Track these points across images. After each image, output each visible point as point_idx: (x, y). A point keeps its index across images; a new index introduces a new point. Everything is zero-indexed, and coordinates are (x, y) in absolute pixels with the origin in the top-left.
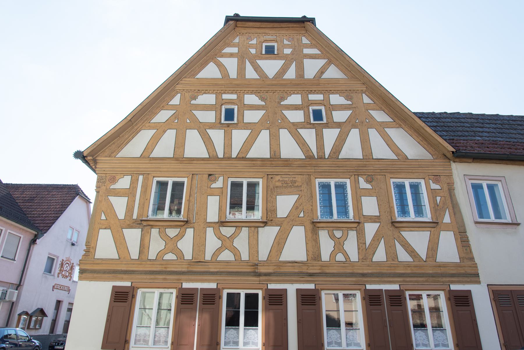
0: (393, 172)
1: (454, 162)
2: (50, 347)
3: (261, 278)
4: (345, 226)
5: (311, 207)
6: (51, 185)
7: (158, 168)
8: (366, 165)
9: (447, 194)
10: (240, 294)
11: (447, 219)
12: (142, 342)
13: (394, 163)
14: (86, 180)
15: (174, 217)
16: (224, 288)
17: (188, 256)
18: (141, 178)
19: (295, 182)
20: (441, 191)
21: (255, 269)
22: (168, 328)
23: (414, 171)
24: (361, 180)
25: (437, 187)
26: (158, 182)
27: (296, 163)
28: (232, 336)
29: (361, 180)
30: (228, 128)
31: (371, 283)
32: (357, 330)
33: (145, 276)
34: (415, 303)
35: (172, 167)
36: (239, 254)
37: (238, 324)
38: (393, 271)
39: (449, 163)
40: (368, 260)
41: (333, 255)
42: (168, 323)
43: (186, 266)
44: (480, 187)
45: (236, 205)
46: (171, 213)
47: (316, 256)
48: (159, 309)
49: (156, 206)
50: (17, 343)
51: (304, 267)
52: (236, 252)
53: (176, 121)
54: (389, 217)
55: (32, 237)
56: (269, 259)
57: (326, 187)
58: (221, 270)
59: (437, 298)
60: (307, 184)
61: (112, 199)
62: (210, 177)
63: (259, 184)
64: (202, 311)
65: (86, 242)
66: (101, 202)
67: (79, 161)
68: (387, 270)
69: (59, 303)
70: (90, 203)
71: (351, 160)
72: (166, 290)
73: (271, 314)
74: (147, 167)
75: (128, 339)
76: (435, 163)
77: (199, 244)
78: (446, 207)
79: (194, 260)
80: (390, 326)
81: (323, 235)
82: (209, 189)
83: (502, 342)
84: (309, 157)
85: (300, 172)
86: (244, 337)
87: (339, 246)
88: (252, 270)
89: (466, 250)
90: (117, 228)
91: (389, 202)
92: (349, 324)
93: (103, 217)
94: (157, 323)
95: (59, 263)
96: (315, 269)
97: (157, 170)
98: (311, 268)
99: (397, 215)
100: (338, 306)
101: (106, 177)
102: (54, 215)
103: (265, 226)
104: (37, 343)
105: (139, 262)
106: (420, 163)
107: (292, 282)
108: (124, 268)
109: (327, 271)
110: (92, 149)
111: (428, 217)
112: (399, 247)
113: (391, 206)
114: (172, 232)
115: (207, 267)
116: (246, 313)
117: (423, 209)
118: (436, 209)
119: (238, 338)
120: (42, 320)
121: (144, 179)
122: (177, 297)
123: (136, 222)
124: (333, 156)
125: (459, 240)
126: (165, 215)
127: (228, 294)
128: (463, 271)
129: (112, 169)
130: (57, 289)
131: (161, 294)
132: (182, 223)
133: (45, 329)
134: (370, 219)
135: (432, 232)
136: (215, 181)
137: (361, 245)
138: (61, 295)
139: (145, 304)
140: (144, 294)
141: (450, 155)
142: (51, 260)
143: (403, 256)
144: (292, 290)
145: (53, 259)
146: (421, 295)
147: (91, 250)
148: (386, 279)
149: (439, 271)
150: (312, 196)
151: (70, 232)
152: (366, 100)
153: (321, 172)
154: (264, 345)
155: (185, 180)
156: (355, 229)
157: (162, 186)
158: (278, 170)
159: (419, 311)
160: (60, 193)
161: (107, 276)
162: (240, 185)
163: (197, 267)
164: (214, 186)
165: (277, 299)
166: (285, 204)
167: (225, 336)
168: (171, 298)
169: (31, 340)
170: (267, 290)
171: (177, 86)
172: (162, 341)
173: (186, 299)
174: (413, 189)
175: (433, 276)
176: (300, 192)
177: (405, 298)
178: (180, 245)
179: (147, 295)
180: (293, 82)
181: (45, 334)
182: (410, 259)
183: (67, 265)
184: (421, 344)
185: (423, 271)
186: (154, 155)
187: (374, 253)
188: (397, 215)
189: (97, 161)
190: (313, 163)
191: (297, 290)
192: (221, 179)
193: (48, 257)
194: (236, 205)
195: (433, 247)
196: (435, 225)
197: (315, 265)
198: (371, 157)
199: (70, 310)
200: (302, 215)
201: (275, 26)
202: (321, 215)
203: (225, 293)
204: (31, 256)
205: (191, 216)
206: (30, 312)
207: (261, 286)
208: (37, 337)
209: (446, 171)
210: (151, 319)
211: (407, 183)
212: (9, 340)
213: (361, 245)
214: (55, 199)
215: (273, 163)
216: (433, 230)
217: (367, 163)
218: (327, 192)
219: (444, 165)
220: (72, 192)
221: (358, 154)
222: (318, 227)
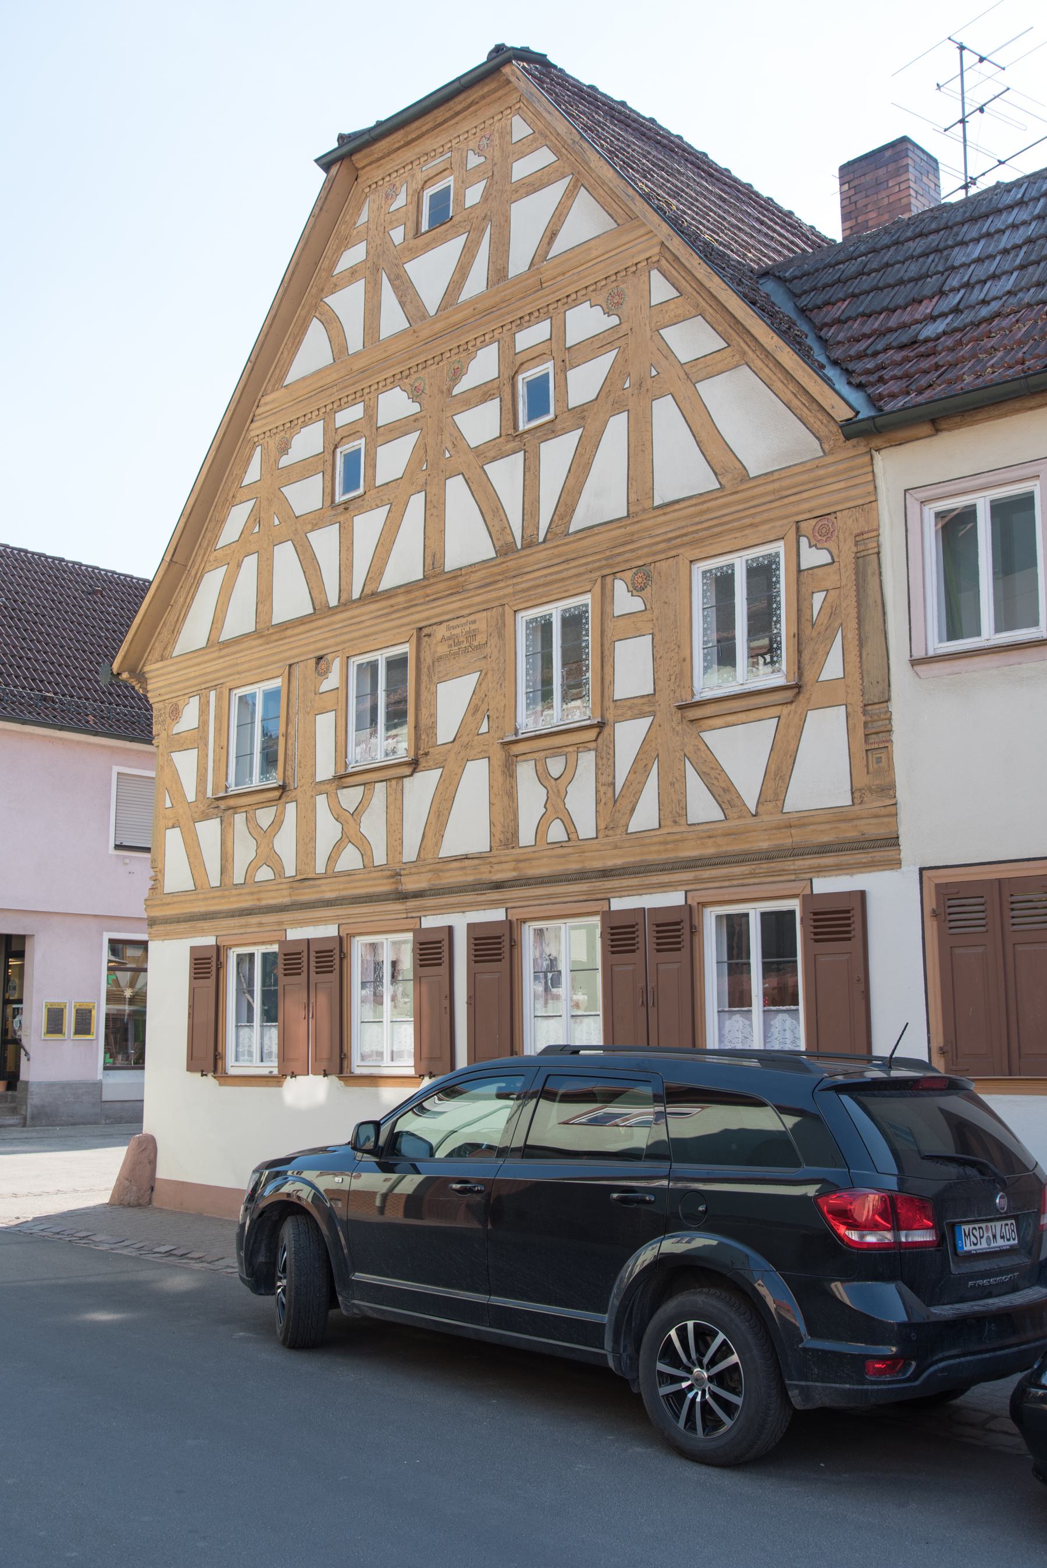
0: (702, 540)
8: (633, 534)
11: (833, 667)
18: (213, 694)
19: (472, 635)
23: (758, 519)
24: (620, 587)
27: (474, 577)
29: (620, 587)
30: (347, 516)
31: (622, 892)
35: (256, 656)
36: (369, 853)
38: (671, 855)
40: (619, 832)
47: (509, 836)
53: (257, 529)
68: (659, 852)
74: (218, 667)
76: (821, 472)
78: (837, 624)
79: (299, 877)
81: (525, 771)
98: (496, 867)
106: (776, 485)
108: (201, 908)
112: (694, 784)
121: (219, 699)
125: (860, 732)
128: (852, 834)
134: (630, 708)
137: (603, 789)
140: (540, 933)
143: (702, 807)
152: (661, 290)
153: (528, 589)
156: (593, 745)
171: (253, 425)
175: (768, 856)
176: (484, 662)
180: (480, 307)
186: (278, 618)
187: (633, 810)
189: (147, 676)
190: (522, 558)
195: (779, 770)
197: (503, 859)
200: (484, 728)
201: (459, 107)
213: (603, 789)
215: (428, 591)
216: (785, 710)
217: (636, 527)
219: (852, 469)
221: (700, 479)
222: (517, 756)
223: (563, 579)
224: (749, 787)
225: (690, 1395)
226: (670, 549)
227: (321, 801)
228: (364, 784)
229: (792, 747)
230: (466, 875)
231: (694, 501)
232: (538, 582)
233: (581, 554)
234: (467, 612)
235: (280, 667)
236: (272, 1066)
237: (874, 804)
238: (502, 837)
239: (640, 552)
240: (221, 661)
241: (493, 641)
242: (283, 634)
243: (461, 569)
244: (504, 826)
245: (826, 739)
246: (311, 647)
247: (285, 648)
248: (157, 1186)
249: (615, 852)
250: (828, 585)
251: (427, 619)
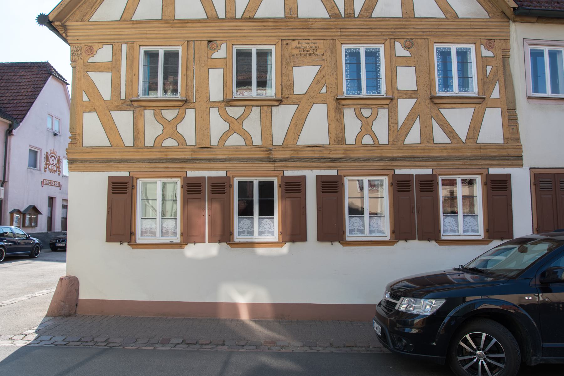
0: (439, 35)
1: (514, 22)
2: (51, 244)
3: (277, 164)
4: (375, 103)
5: (335, 81)
6: (16, 63)
7: (144, 34)
8: (406, 25)
9: (499, 63)
10: (252, 182)
11: (496, 94)
12: (148, 234)
13: (440, 23)
14: (55, 52)
15: (170, 96)
16: (234, 177)
17: (191, 140)
18: (124, 47)
19: (316, 49)
20: (493, 59)
21: (269, 154)
22: (176, 219)
23: (463, 34)
24: (398, 45)
25: (490, 54)
26: (146, 53)
27: (317, 24)
28: (246, 226)
29: (398, 45)
31: (401, 167)
32: (382, 218)
33: (143, 165)
34: (449, 188)
35: (162, 32)
36: (250, 138)
37: (252, 214)
38: (426, 154)
39: (507, 24)
40: (400, 143)
41: (359, 137)
42: (176, 214)
43: (190, 153)
44: (541, 53)
45: (243, 83)
46: (165, 91)
47: (340, 139)
48: (164, 199)
49: (147, 85)
50: (15, 240)
51: (325, 152)
52: (246, 135)
54: (428, 92)
55: (6, 127)
56: (285, 143)
57: (354, 55)
58: (230, 156)
59: (473, 183)
60: (331, 52)
61: (93, 75)
62: (210, 44)
63: (271, 52)
64: (211, 201)
65: (70, 129)
66: (79, 79)
67: (45, 29)
68: (420, 153)
69: (51, 200)
70: (67, 84)
71: (387, 19)
72: (169, 179)
73: (288, 202)
75: (133, 231)
76: (490, 24)
77: (203, 127)
78: (496, 79)
79: (197, 146)
80: (418, 212)
81: (349, 114)
82: (209, 60)
83: (535, 226)
84: (335, 16)
85: (322, 36)
86: (259, 226)
87: (367, 127)
88: (266, 156)
89: (513, 129)
90: (105, 111)
91: (429, 74)
92: (373, 214)
93: (85, 98)
94: (163, 214)
95: (43, 156)
96: (338, 154)
97: (143, 36)
98: (333, 152)
99: (437, 89)
100: (362, 194)
101: (81, 47)
102: (26, 101)
103: (279, 104)
104: (37, 241)
105: (135, 150)
106: (472, 23)
107: (311, 168)
108: (118, 156)
109: (352, 156)
110: (59, 11)
111: (474, 90)
112: (437, 129)
113: (431, 78)
114: (170, 114)
115: (214, 153)
116: (260, 202)
117: (470, 82)
118: (486, 82)
119: (253, 228)
120: (37, 218)
121: (128, 49)
122: (182, 187)
123: (125, 102)
124: (365, 15)
125: (506, 118)
126: (160, 94)
127: (239, 182)
129: (86, 37)
130: (47, 184)
131: (164, 184)
132: (180, 103)
133: (42, 226)
134: (405, 94)
135: (476, 109)
136: (216, 49)
137: (392, 125)
138: (53, 191)
139: (148, 195)
140: (145, 184)
141: (510, 13)
142: (34, 154)
143: (440, 137)
144: (311, 176)
145: (36, 152)
146: (456, 180)
147: (78, 137)
148: (418, 163)
149: (479, 154)
150: (337, 67)
151: (49, 120)
153: (348, 36)
154: (281, 233)
155: (179, 49)
156: (387, 106)
157: (152, 56)
158: (295, 34)
159: (452, 198)
160: (29, 73)
161: (100, 165)
162: (248, 54)
163: (202, 153)
164: (215, 55)
165: (294, 187)
166: (304, 77)
167: (239, 226)
168: (175, 188)
169: (29, 237)
170: (283, 177)
172: (170, 232)
173: (192, 189)
174: (460, 57)
175: (470, 158)
176: (322, 62)
177: (438, 183)
178: (180, 128)
179: (149, 186)
181: (43, 232)
182: (448, 141)
183: (53, 158)
184: (449, 229)
185: (461, 154)
186: (137, 16)
187: (407, 135)
188: (437, 89)
189: (68, 27)
191: (317, 177)
192: (224, 46)
193: (30, 150)
194: (243, 83)
195: (475, 127)
196: (481, 100)
197: (338, 149)
198: (412, 15)
199: (65, 207)
200: (324, 90)
202: (347, 90)
203: (236, 181)
204: (10, 149)
205: (190, 94)
206: (22, 210)
207: (276, 173)
208: (35, 235)
209: (502, 34)
210: (156, 211)
211: (454, 48)
212: (7, 238)
213: (392, 125)
214: (24, 80)
215: (289, 24)
216: (477, 106)
217: (407, 23)
218: (355, 62)
219: (502, 26)
220: (42, 72)
222: (343, 105)
223: (368, 36)
224: (462, 133)
225: (480, 363)
226: (423, 35)
228: (245, 106)
229: (480, 120)
230: (315, 154)
231: (435, 20)
232: (354, 33)
233: (379, 27)
234: (312, 38)
235: (181, 41)
236: (178, 239)
237: (512, 144)
238: (335, 139)
239: (409, 33)
240: (133, 30)
241: (328, 54)
242: (185, 25)
243: (310, 18)
244: (336, 135)
245: (493, 120)
246: (206, 35)
247: (185, 32)
248: (79, 303)
249: (399, 151)
250: (493, 64)
251: (287, 36)
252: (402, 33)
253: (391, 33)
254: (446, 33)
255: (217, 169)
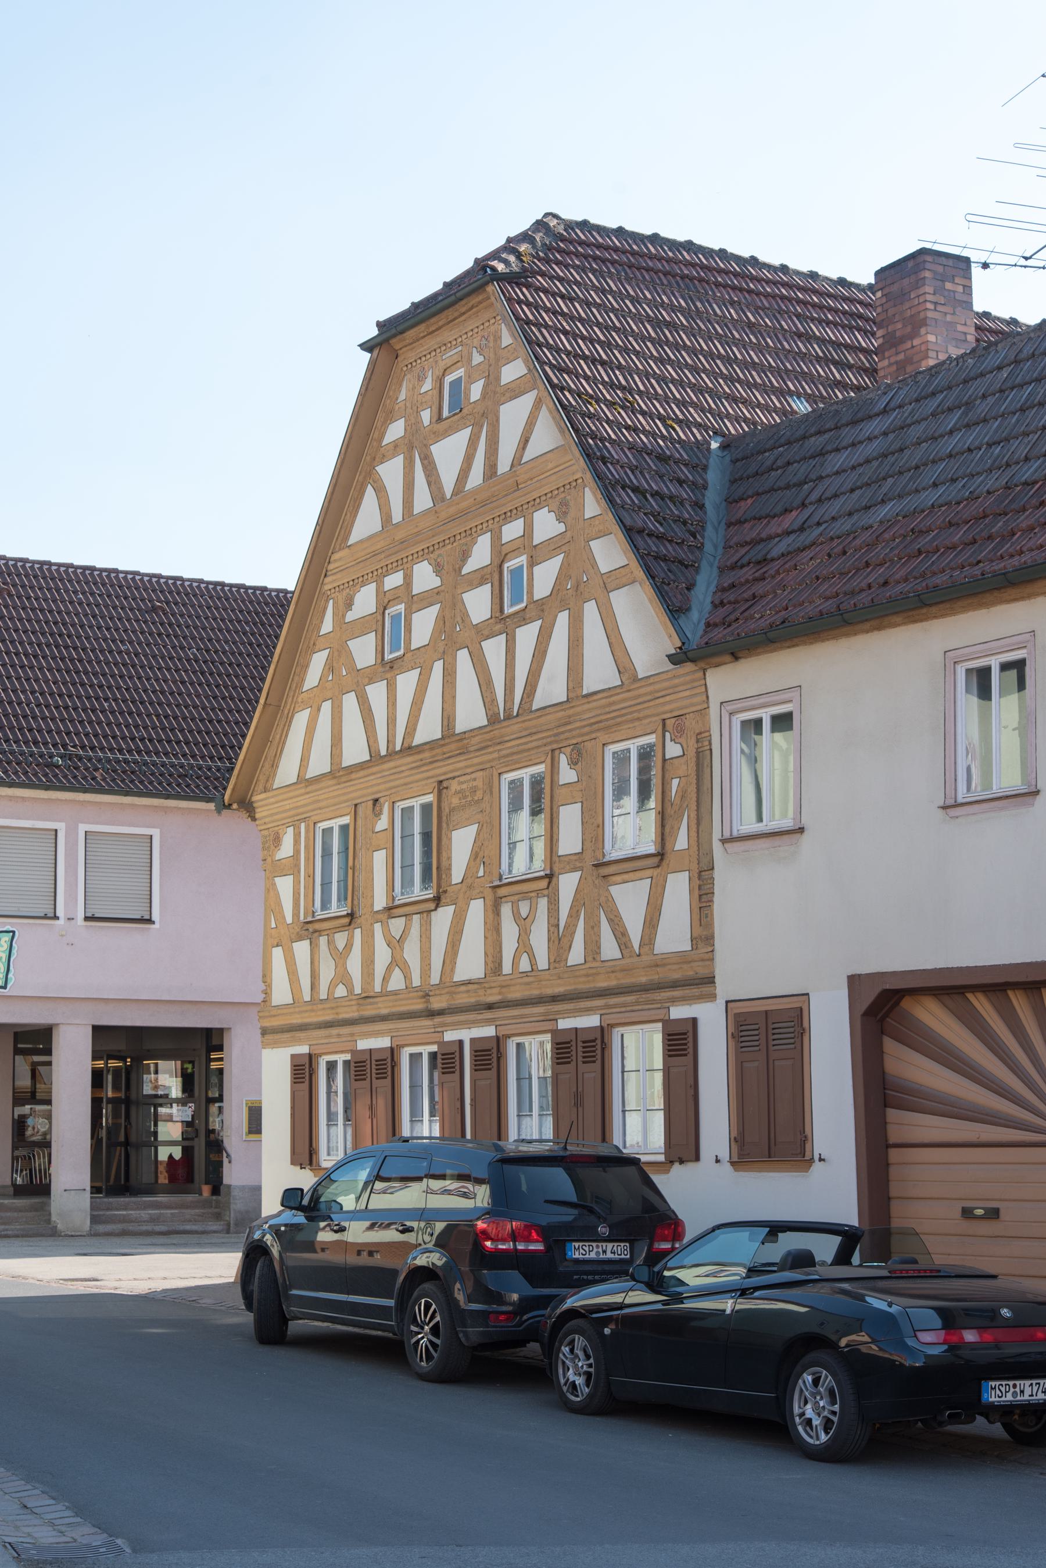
8: (569, 717)
16: (404, 1046)
18: (303, 825)
23: (641, 715)
38: (592, 985)
76: (676, 681)
125: (696, 893)
171: (327, 580)
175: (645, 988)
189: (255, 805)
227: (378, 927)
246: (369, 791)
247: (352, 789)
250: (681, 773)
252: (567, 735)
253: (553, 739)
254: (619, 720)
255: (589, 1011)
